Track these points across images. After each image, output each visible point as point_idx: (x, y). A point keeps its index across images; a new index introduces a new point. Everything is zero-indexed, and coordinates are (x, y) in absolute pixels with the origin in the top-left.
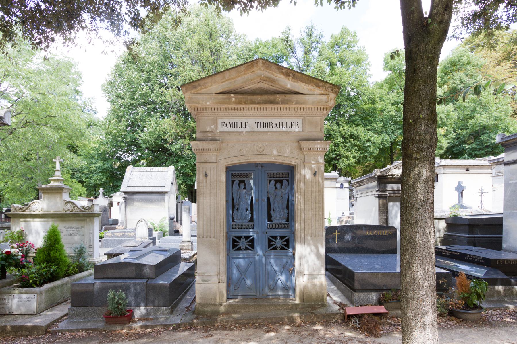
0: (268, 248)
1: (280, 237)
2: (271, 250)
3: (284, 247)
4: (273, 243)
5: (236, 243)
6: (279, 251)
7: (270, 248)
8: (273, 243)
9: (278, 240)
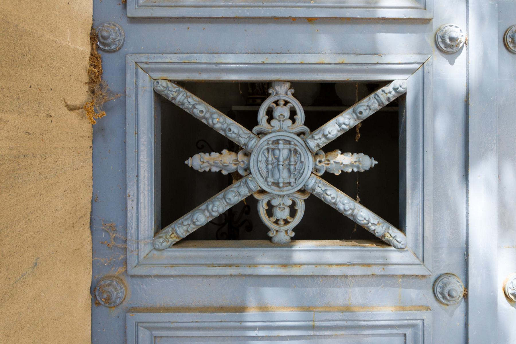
3: (220, 122)
4: (345, 161)
5: (200, 162)
8: (345, 161)
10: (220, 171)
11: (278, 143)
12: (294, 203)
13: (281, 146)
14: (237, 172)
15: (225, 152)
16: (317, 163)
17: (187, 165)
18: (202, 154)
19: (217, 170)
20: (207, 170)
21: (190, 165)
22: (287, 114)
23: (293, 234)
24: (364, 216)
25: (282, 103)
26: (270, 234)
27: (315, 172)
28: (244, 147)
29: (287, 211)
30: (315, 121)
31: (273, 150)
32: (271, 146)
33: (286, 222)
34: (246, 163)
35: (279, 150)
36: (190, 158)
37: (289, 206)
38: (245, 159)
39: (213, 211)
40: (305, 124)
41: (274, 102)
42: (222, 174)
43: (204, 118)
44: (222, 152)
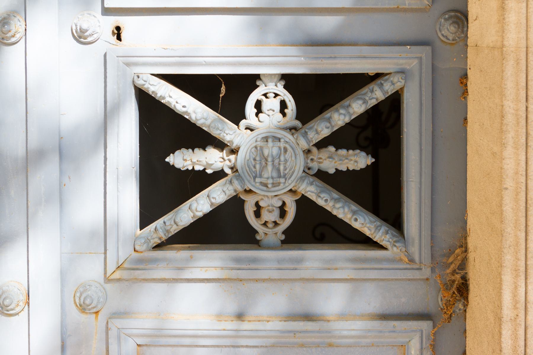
0: (394, 103)
1: (290, 81)
2: (354, 83)
3: (343, 210)
4: (209, 159)
5: (359, 160)
6: (271, 260)
7: (376, 95)
8: (209, 159)
9: (269, 111)
10: (205, 169)
11: (273, 183)
12: (284, 204)
13: (270, 181)
14: (222, 170)
15: (332, 171)
16: (309, 161)
17: (373, 157)
18: (184, 150)
19: (201, 168)
20: (190, 168)
21: (171, 163)
22: (277, 107)
23: (283, 237)
24: (364, 223)
25: (270, 225)
26: (258, 238)
27: (307, 170)
28: (229, 144)
29: (277, 213)
30: (235, 204)
31: (280, 177)
32: (282, 180)
33: (276, 224)
34: (233, 161)
35: (272, 178)
36: (171, 155)
37: (280, 207)
38: (311, 165)
39: (197, 211)
40: (297, 118)
41: (279, 224)
42: (206, 173)
43: (186, 113)
44: (334, 171)
